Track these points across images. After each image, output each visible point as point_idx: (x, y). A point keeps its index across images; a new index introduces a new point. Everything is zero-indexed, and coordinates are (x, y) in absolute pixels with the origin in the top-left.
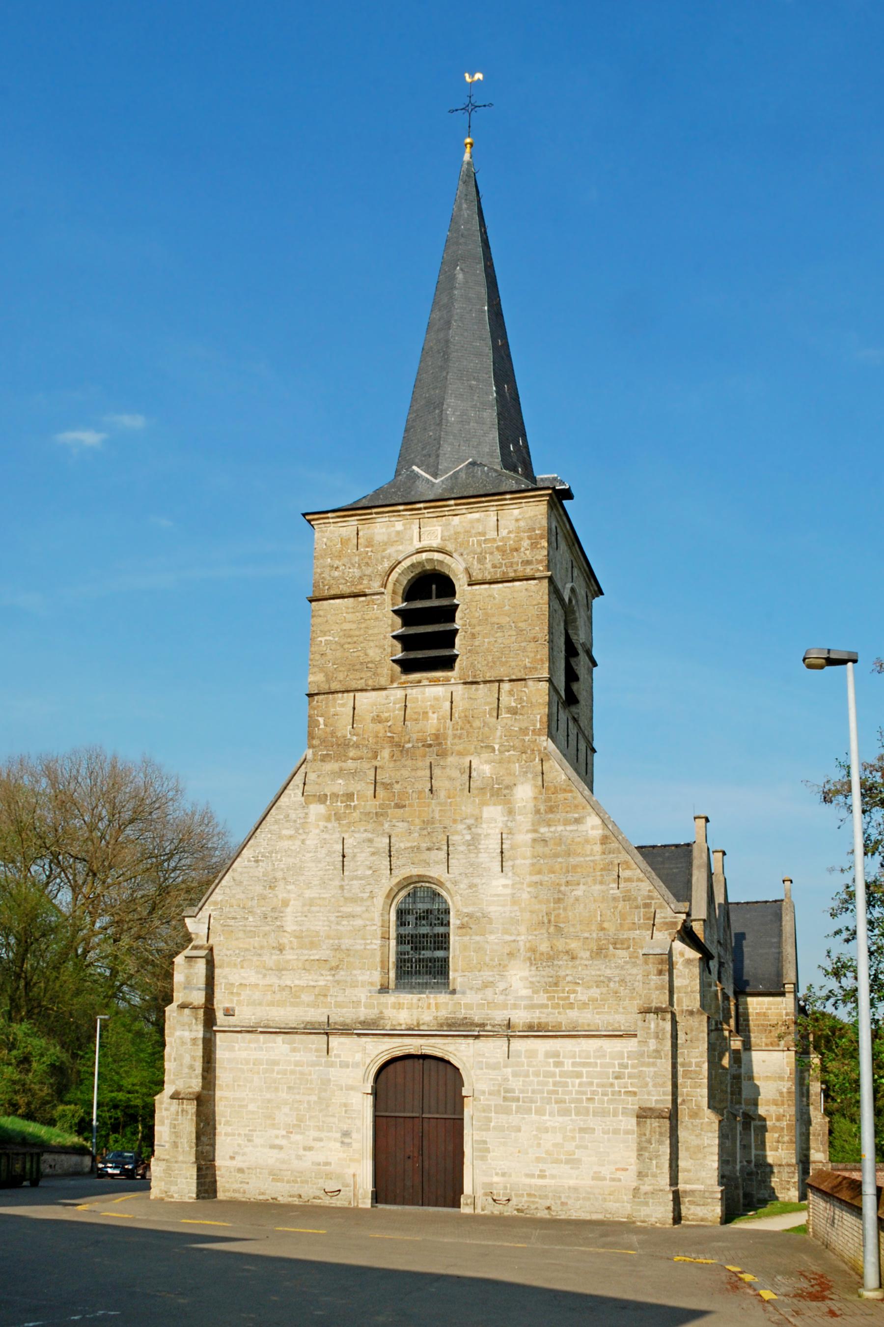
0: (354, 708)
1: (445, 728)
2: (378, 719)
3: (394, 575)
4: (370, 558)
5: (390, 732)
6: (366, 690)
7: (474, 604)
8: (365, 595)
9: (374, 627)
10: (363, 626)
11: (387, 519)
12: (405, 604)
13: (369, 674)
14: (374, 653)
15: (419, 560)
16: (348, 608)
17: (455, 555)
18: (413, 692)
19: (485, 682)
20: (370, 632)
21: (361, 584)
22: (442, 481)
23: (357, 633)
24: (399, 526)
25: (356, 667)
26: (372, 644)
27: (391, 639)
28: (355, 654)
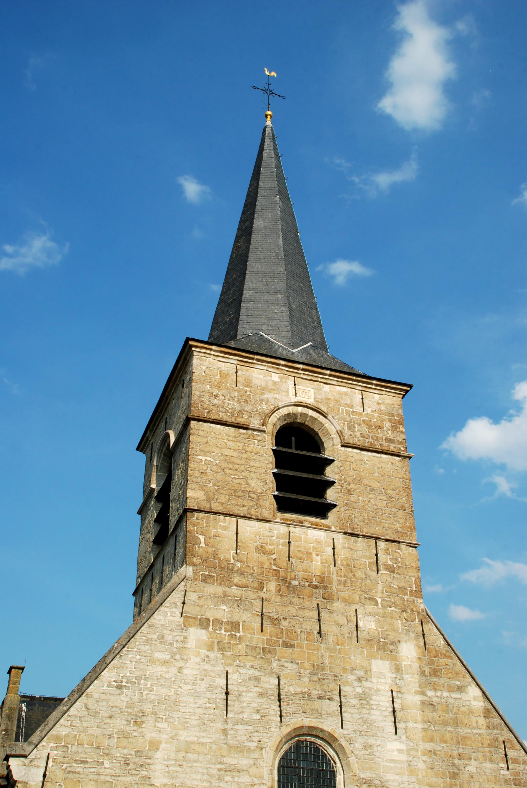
0: (237, 534)
1: (329, 573)
2: (262, 550)
4: (249, 396)
6: (249, 518)
8: (247, 429)
9: (255, 460)
10: (244, 456)
11: (266, 368)
13: (252, 504)
14: (255, 484)
16: (229, 436)
17: (330, 417)
18: (296, 531)
19: (364, 536)
20: (252, 464)
21: (241, 417)
23: (238, 461)
24: (275, 377)
25: (238, 494)
26: (253, 475)
28: (237, 481)
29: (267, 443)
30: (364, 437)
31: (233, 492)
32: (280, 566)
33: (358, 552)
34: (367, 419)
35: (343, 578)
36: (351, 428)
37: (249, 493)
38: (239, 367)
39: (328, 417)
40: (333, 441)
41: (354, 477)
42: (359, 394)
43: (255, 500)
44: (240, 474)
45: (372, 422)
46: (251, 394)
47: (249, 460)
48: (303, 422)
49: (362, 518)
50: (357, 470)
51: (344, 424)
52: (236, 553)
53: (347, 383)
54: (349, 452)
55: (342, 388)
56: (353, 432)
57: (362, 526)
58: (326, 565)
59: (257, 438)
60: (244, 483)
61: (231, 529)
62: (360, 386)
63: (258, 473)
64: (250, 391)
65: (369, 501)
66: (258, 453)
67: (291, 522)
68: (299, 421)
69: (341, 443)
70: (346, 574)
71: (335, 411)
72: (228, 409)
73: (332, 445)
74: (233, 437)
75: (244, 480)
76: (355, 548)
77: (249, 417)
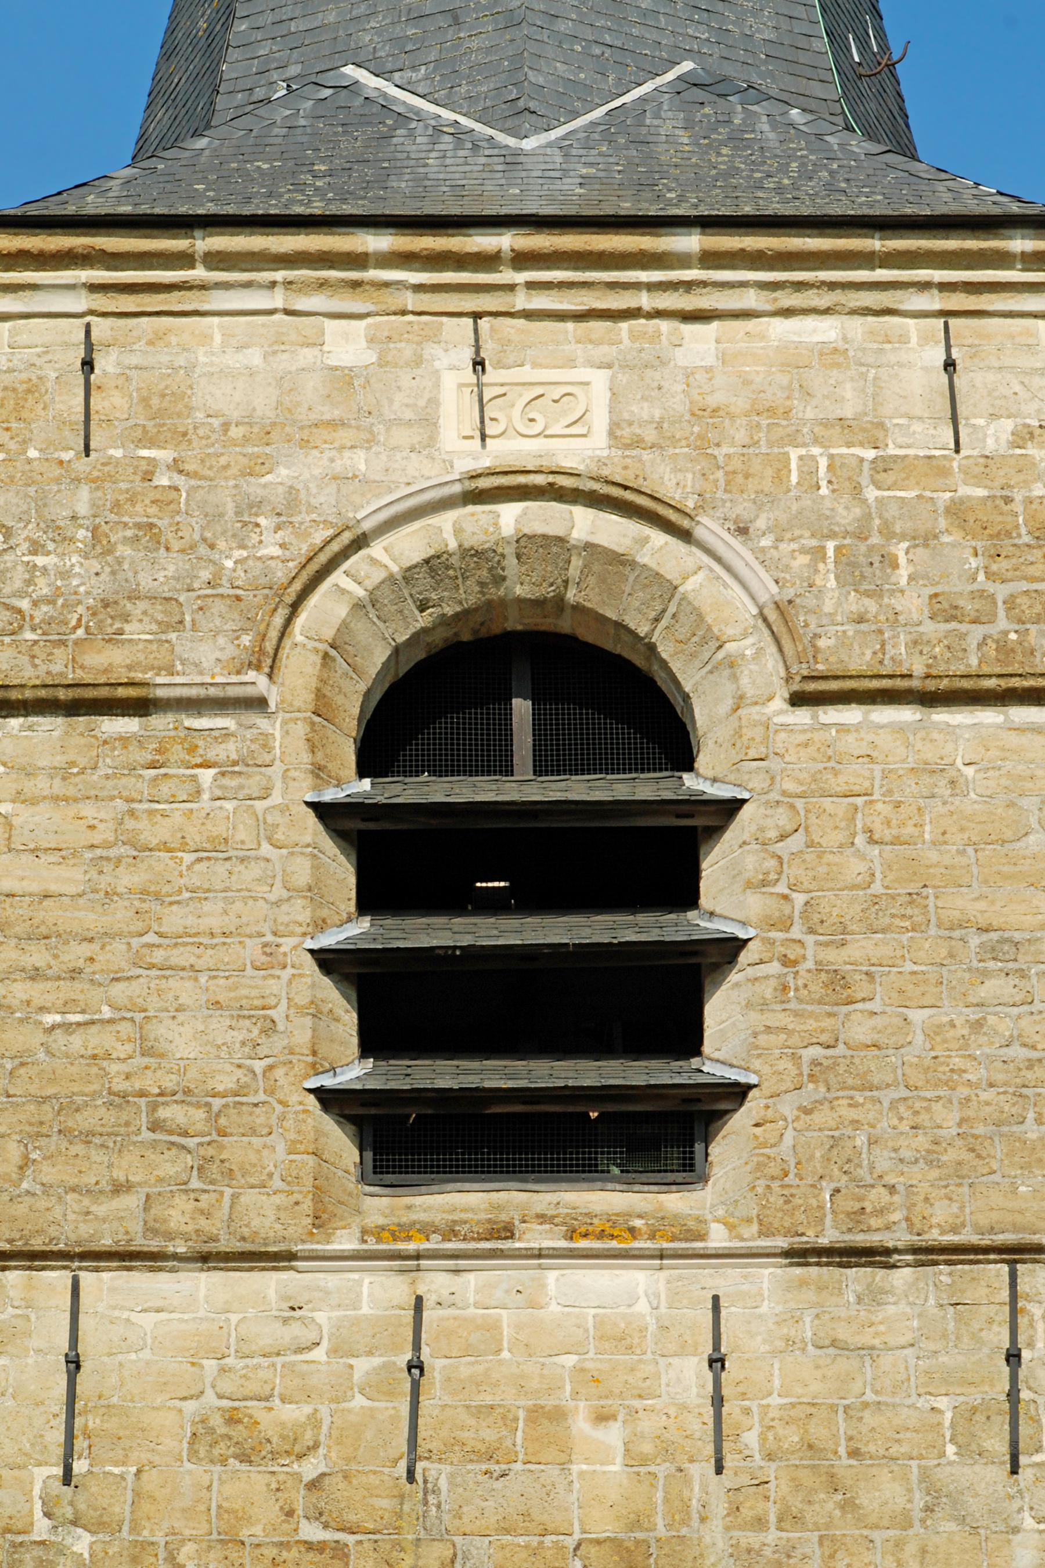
0: (74, 1363)
1: (680, 1511)
2: (233, 1437)
3: (326, 609)
4: (166, 500)
5: (317, 1515)
6: (152, 1259)
7: (838, 807)
8: (141, 706)
9: (201, 894)
10: (127, 879)
11: (277, 299)
12: (366, 784)
13: (171, 1166)
14: (195, 1043)
15: (475, 539)
16: (29, 772)
17: (709, 528)
18: (463, 1293)
19: (927, 1254)
20: (175, 919)
21: (114, 639)
22: (562, 146)
23: (90, 919)
24: (348, 345)
25: (85, 1120)
26: (184, 990)
27: (310, 965)
28: (76, 1042)
29: (278, 768)
30: (953, 614)
31: (48, 1112)
32: (352, 1518)
33: (886, 1361)
34: (981, 492)
35: (772, 1536)
36: (865, 570)
37: (154, 1107)
38: (101, 328)
39: (699, 532)
40: (734, 678)
41: (877, 888)
42: (925, 339)
43: (191, 1142)
44: (96, 994)
45: (1018, 507)
46: (180, 481)
47: (158, 897)
48: (549, 592)
49: (922, 1141)
50: (896, 841)
51: (819, 553)
52: (67, 1478)
53: (832, 286)
54: (843, 729)
55: (810, 322)
56: (876, 594)
57: (924, 1188)
58: (662, 1469)
59: (211, 755)
60: (122, 1050)
61: (35, 1342)
62: (924, 286)
63: (213, 972)
64: (177, 466)
65: (977, 1025)
66: (216, 849)
67: (434, 1243)
68: (519, 591)
69: (788, 679)
70: (796, 1503)
71: (752, 485)
72: (25, 604)
73: (729, 702)
74: (54, 772)
75: (125, 1028)
76: (866, 1338)
77: (165, 627)
